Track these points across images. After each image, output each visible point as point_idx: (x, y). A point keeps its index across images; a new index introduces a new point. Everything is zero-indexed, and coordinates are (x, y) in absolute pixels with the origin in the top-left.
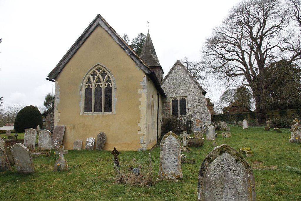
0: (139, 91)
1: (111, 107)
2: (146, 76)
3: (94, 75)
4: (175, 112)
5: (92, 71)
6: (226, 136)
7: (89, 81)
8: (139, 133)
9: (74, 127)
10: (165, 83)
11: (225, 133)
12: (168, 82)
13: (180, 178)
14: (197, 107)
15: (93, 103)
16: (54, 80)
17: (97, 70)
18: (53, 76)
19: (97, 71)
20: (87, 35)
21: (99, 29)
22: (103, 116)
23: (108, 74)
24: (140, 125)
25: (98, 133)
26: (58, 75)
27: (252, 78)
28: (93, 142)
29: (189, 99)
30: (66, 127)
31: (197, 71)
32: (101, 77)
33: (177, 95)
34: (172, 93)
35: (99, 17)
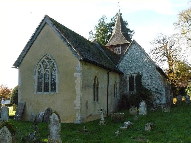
0: (75, 75)
5: (42, 59)
8: (75, 108)
9: (31, 104)
10: (122, 61)
12: (125, 60)
14: (151, 82)
17: (46, 58)
18: (17, 64)
19: (45, 60)
22: (50, 95)
23: (54, 61)
24: (75, 102)
25: (47, 108)
28: (43, 115)
31: (174, 43)
33: (133, 72)
34: (128, 70)
35: (46, 17)
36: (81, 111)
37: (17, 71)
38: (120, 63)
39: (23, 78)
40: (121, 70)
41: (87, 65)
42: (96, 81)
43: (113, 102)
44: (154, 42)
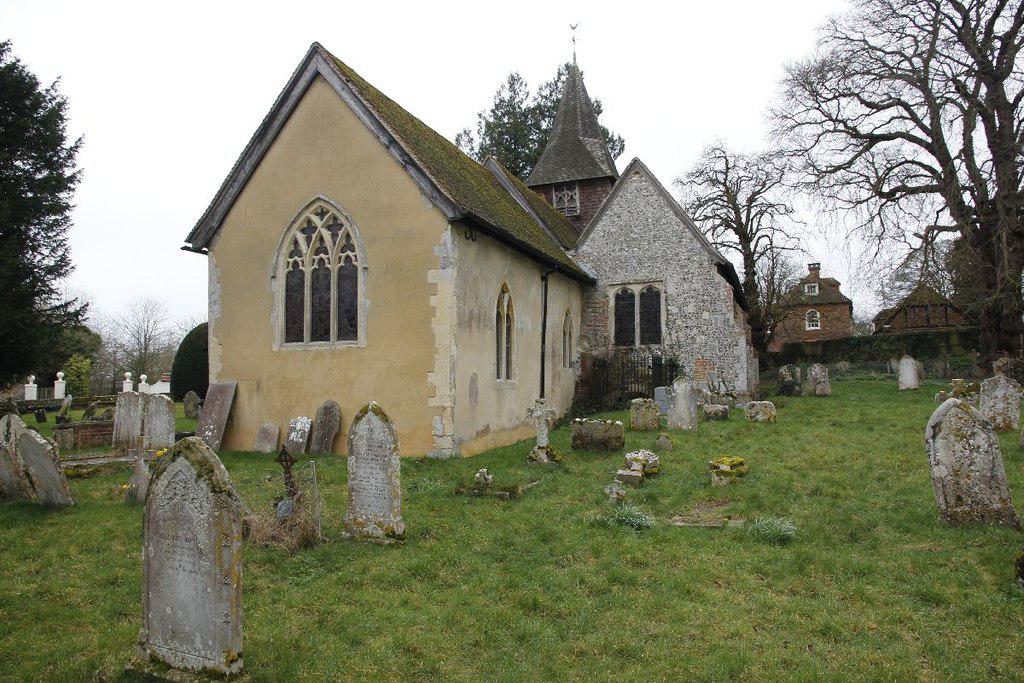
0: (433, 276)
1: (356, 326)
2: (450, 226)
3: (309, 229)
4: (624, 335)
5: (303, 217)
6: (760, 417)
7: (296, 251)
8: (432, 402)
11: (753, 405)
13: (394, 533)
14: (697, 315)
15: (307, 316)
16: (204, 249)
17: (317, 214)
18: (202, 238)
19: (316, 220)
20: (285, 110)
21: (318, 89)
22: (333, 353)
24: (432, 378)
25: (321, 403)
26: (213, 235)
27: (967, 197)
29: (672, 290)
30: (237, 386)
31: (764, 185)
32: (327, 235)
33: (631, 279)
35: (316, 50)
36: (453, 413)
37: (201, 262)
38: (583, 243)
39: (222, 287)
40: (587, 268)
41: (473, 240)
42: (505, 304)
43: (564, 382)
44: (692, 178)
